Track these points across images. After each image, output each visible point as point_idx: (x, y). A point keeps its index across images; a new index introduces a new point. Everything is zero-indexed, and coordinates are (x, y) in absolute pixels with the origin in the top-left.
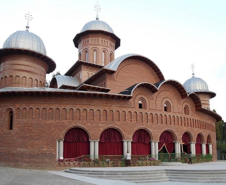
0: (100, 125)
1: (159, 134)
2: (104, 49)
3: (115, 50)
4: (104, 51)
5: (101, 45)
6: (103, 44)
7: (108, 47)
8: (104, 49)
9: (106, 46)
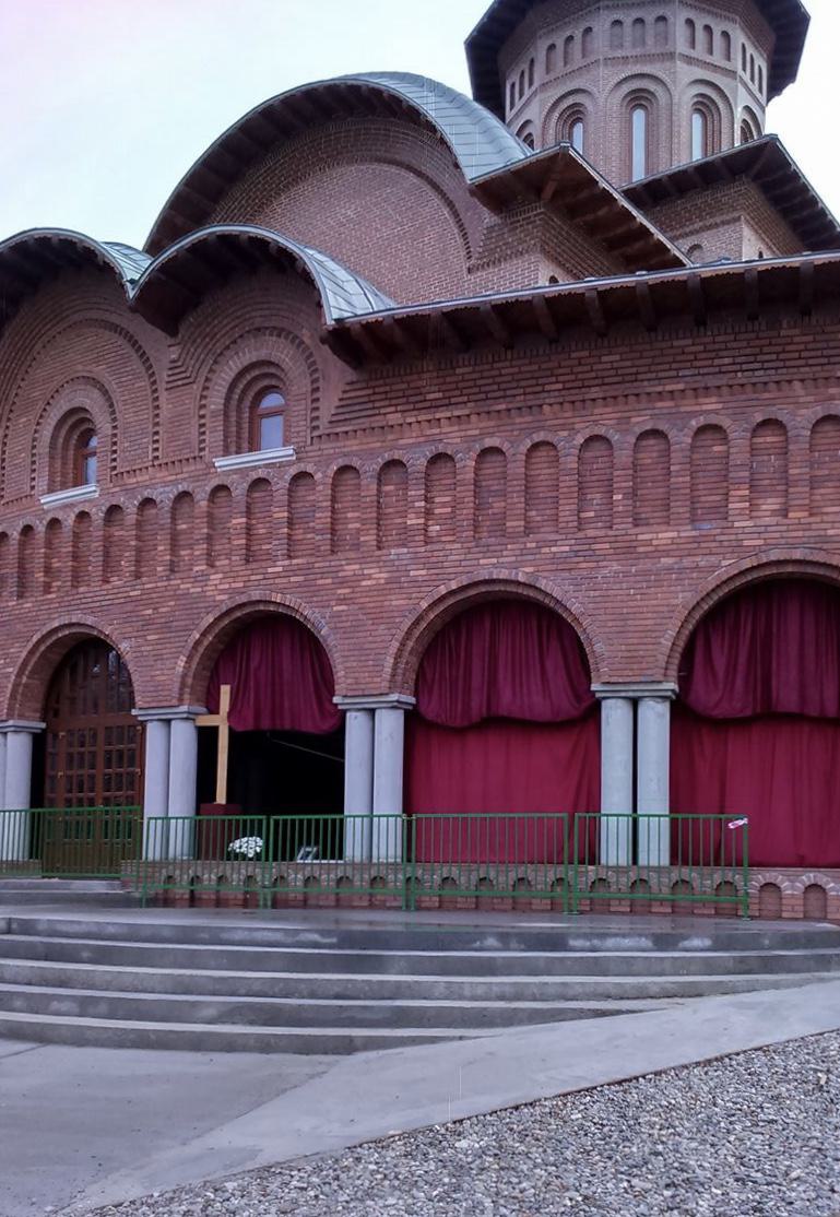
1: (7, 676)
2: (626, 88)
3: (769, 100)
4: (704, 107)
5: (689, 60)
6: (699, 52)
7: (732, 74)
9: (715, 68)
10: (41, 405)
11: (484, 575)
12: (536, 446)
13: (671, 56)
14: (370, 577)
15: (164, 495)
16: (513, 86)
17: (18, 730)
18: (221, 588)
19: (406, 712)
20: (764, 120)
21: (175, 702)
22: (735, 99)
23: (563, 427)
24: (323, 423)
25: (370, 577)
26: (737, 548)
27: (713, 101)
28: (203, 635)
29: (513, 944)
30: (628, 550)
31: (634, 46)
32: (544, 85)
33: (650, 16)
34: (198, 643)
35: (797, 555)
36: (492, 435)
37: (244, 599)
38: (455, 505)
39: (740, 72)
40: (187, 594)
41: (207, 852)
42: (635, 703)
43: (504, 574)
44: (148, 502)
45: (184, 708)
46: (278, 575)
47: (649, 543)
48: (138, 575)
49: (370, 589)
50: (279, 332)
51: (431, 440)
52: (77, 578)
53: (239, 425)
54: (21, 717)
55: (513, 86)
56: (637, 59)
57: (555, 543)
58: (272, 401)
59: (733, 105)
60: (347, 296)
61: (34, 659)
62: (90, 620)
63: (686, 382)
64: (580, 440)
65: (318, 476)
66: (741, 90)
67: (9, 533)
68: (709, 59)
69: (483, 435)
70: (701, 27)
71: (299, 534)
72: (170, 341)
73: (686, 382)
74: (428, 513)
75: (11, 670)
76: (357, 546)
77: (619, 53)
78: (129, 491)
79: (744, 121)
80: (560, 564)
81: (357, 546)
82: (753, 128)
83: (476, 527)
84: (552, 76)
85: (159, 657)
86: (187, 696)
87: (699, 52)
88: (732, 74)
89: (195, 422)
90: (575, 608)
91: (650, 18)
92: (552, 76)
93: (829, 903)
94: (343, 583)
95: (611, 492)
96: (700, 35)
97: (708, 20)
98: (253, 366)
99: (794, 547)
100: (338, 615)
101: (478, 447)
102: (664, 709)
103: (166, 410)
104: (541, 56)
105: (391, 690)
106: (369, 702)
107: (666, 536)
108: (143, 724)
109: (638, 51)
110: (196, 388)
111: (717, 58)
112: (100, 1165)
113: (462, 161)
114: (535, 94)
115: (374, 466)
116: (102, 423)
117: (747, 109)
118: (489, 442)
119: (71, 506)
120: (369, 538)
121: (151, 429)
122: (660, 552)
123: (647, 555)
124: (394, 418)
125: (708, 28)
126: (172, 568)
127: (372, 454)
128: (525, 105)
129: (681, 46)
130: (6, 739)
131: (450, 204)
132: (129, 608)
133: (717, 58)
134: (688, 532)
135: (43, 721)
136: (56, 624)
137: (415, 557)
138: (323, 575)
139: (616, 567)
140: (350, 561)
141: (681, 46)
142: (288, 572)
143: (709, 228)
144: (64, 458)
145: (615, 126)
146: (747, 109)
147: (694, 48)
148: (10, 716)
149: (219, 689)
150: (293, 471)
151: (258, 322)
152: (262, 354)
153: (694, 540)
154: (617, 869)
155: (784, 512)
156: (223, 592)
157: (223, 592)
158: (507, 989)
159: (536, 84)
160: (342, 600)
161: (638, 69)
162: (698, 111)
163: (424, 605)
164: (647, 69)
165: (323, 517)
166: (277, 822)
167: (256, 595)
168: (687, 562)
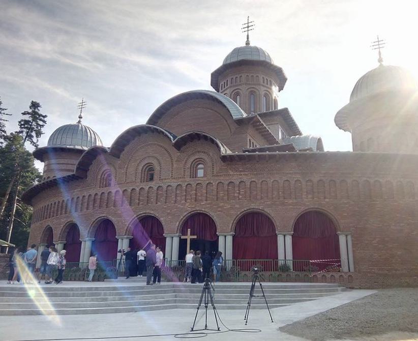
0: (62, 220)
2: (250, 90)
5: (263, 86)
8: (250, 90)
10: (139, 161)
12: (262, 181)
13: (260, 85)
15: (174, 185)
16: (222, 85)
18: (188, 208)
24: (215, 173)
28: (184, 217)
29: (72, 294)
32: (230, 87)
34: (182, 219)
35: (316, 207)
36: (253, 178)
38: (245, 192)
42: (285, 236)
43: (257, 207)
45: (178, 234)
48: (166, 202)
53: (193, 171)
54: (128, 235)
55: (222, 85)
57: (267, 201)
58: (200, 166)
60: (225, 151)
61: (133, 221)
62: (152, 212)
64: (272, 181)
65: (214, 184)
67: (127, 189)
71: (208, 196)
72: (178, 151)
74: (239, 193)
76: (223, 199)
78: (137, 186)
81: (223, 199)
83: (250, 197)
84: (232, 85)
86: (178, 232)
92: (232, 85)
94: (220, 207)
98: (196, 159)
101: (250, 180)
102: (291, 237)
103: (175, 166)
105: (231, 232)
106: (225, 234)
108: (165, 238)
113: (232, 115)
114: (228, 88)
115: (227, 183)
116: (157, 168)
118: (253, 180)
120: (226, 198)
121: (171, 170)
125: (263, 78)
126: (175, 202)
134: (295, 201)
136: (141, 213)
140: (221, 203)
143: (272, 124)
148: (125, 235)
151: (199, 150)
152: (201, 157)
154: (346, 273)
155: (313, 198)
156: (189, 208)
157: (189, 208)
159: (229, 86)
160: (219, 211)
163: (239, 213)
165: (215, 193)
166: (239, 261)
167: (198, 209)
168: (295, 207)
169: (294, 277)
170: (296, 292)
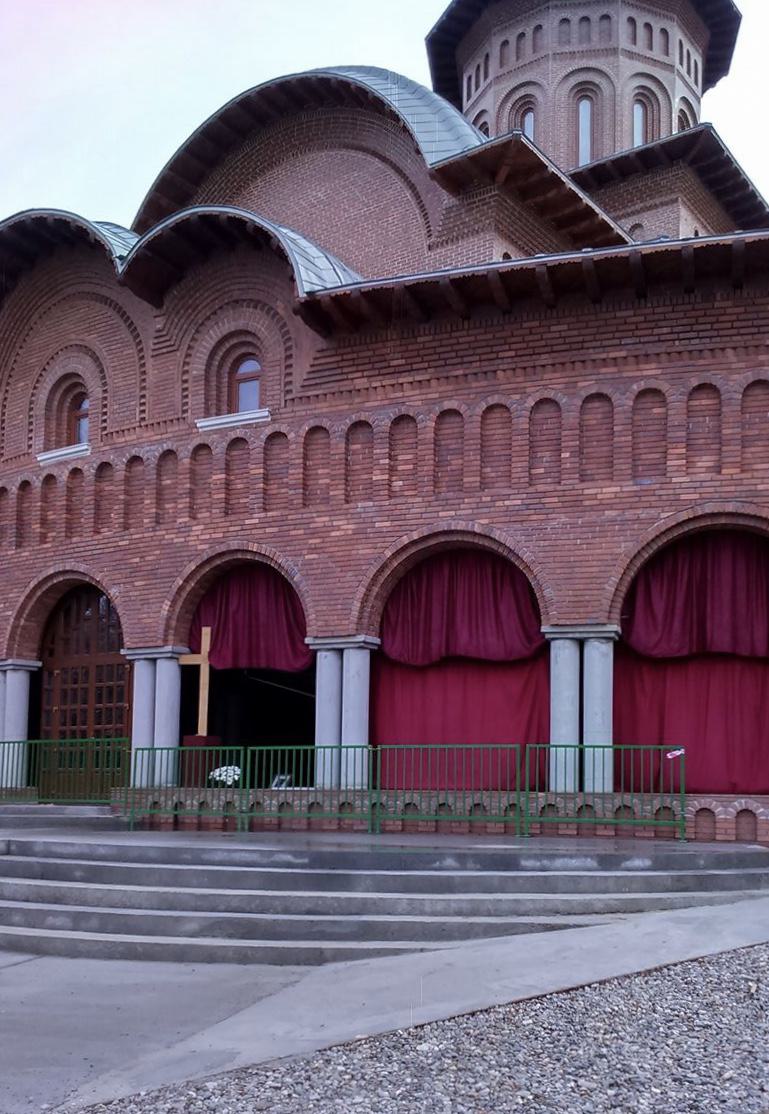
1: (7, 619)
2: (573, 81)
3: (704, 92)
4: (645, 98)
5: (631, 55)
6: (640, 48)
7: (670, 67)
9: (655, 62)
10: (38, 370)
11: (443, 526)
12: (490, 409)
13: (614, 51)
14: (338, 528)
15: (151, 453)
16: (470, 78)
17: (16, 668)
18: (202, 538)
19: (372, 651)
20: (699, 110)
21: (160, 643)
22: (673, 90)
23: (515, 391)
24: (296, 387)
25: (338, 528)
26: (675, 502)
27: (653, 93)
28: (186, 581)
30: (575, 504)
31: (580, 42)
32: (498, 78)
33: (595, 14)
34: (181, 588)
35: (730, 508)
36: (450, 398)
37: (223, 548)
38: (417, 462)
39: (677, 65)
40: (171, 544)
41: (190, 780)
42: (581, 643)
43: (461, 526)
44: (135, 460)
45: (169, 648)
46: (254, 527)
47: (594, 497)
48: (126, 527)
49: (339, 539)
50: (256, 304)
51: (395, 403)
52: (70, 529)
53: (219, 389)
54: (19, 656)
55: (470, 78)
56: (583, 54)
57: (508, 497)
58: (249, 367)
59: (671, 96)
60: (318, 271)
61: (31, 603)
62: (82, 568)
63: (628, 350)
64: (531, 402)
65: (291, 436)
66: (679, 82)
67: (8, 488)
68: (649, 54)
69: (442, 398)
70: (642, 25)
71: (273, 489)
72: (156, 312)
73: (628, 350)
74: (392, 470)
75: (10, 613)
76: (327, 500)
77: (567, 49)
78: (118, 450)
79: (681, 110)
80: (513, 516)
81: (327, 500)
82: (689, 118)
83: (436, 483)
84: (505, 70)
85: (145, 602)
86: (171, 637)
87: (640, 48)
88: (670, 67)
89: (179, 386)
90: (527, 556)
91: (595, 16)
92: (505, 70)
93: (759, 826)
94: (314, 533)
95: (560, 451)
96: (641, 32)
97: (649, 19)
98: (231, 335)
99: (727, 500)
100: (309, 563)
101: (437, 410)
102: (608, 649)
103: (152, 375)
104: (495, 51)
105: (358, 632)
106: (338, 643)
107: (610, 490)
108: (131, 663)
109: (584, 47)
110: (180, 355)
111: (657, 53)
112: (92, 1066)
113: (423, 147)
114: (489, 86)
115: (343, 426)
116: (94, 387)
117: (684, 100)
118: (448, 405)
119: (65, 463)
120: (338, 493)
121: (138, 393)
122: (604, 505)
123: (592, 508)
124: (361, 383)
125: (648, 26)
126: (158, 520)
127: (341, 415)
128: (481, 96)
129: (624, 42)
130: (5, 676)
131: (412, 187)
132: (118, 556)
133: (657, 53)
134: (630, 487)
135: (40, 660)
136: (51, 571)
137: (380, 510)
138: (296, 526)
139: (564, 519)
140: (320, 514)
141: (624, 42)
142: (264, 524)
143: (649, 208)
144: (59, 419)
145: (563, 116)
146: (684, 100)
147: (635, 44)
148: (9, 655)
149: (201, 631)
150: (268, 431)
151: (236, 295)
152: (240, 324)
153: (636, 494)
155: (718, 469)
156: (204, 542)
157: (204, 542)
158: (464, 906)
159: (491, 77)
160: (313, 549)
161: (584, 63)
162: (639, 101)
163: (388, 554)
164: (592, 63)
165: (296, 473)
166: (253, 752)
167: (234, 545)
168: (629, 514)
169: (609, 815)
170: (271, 931)
